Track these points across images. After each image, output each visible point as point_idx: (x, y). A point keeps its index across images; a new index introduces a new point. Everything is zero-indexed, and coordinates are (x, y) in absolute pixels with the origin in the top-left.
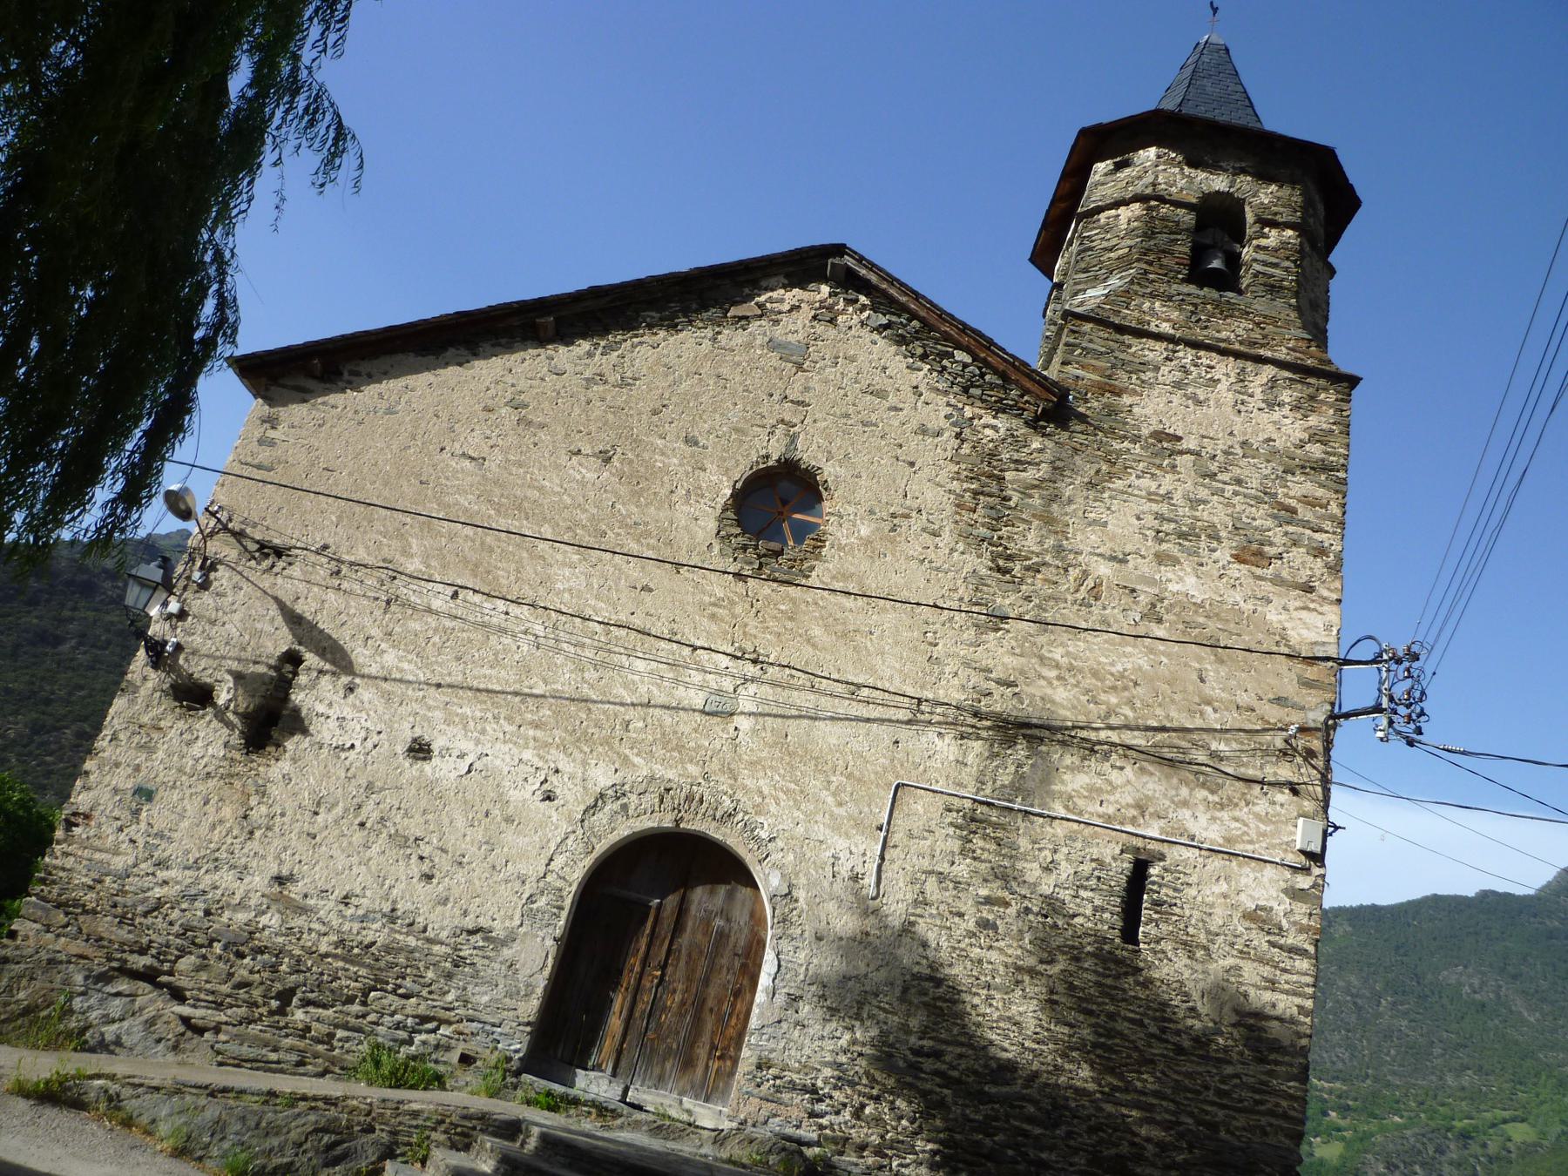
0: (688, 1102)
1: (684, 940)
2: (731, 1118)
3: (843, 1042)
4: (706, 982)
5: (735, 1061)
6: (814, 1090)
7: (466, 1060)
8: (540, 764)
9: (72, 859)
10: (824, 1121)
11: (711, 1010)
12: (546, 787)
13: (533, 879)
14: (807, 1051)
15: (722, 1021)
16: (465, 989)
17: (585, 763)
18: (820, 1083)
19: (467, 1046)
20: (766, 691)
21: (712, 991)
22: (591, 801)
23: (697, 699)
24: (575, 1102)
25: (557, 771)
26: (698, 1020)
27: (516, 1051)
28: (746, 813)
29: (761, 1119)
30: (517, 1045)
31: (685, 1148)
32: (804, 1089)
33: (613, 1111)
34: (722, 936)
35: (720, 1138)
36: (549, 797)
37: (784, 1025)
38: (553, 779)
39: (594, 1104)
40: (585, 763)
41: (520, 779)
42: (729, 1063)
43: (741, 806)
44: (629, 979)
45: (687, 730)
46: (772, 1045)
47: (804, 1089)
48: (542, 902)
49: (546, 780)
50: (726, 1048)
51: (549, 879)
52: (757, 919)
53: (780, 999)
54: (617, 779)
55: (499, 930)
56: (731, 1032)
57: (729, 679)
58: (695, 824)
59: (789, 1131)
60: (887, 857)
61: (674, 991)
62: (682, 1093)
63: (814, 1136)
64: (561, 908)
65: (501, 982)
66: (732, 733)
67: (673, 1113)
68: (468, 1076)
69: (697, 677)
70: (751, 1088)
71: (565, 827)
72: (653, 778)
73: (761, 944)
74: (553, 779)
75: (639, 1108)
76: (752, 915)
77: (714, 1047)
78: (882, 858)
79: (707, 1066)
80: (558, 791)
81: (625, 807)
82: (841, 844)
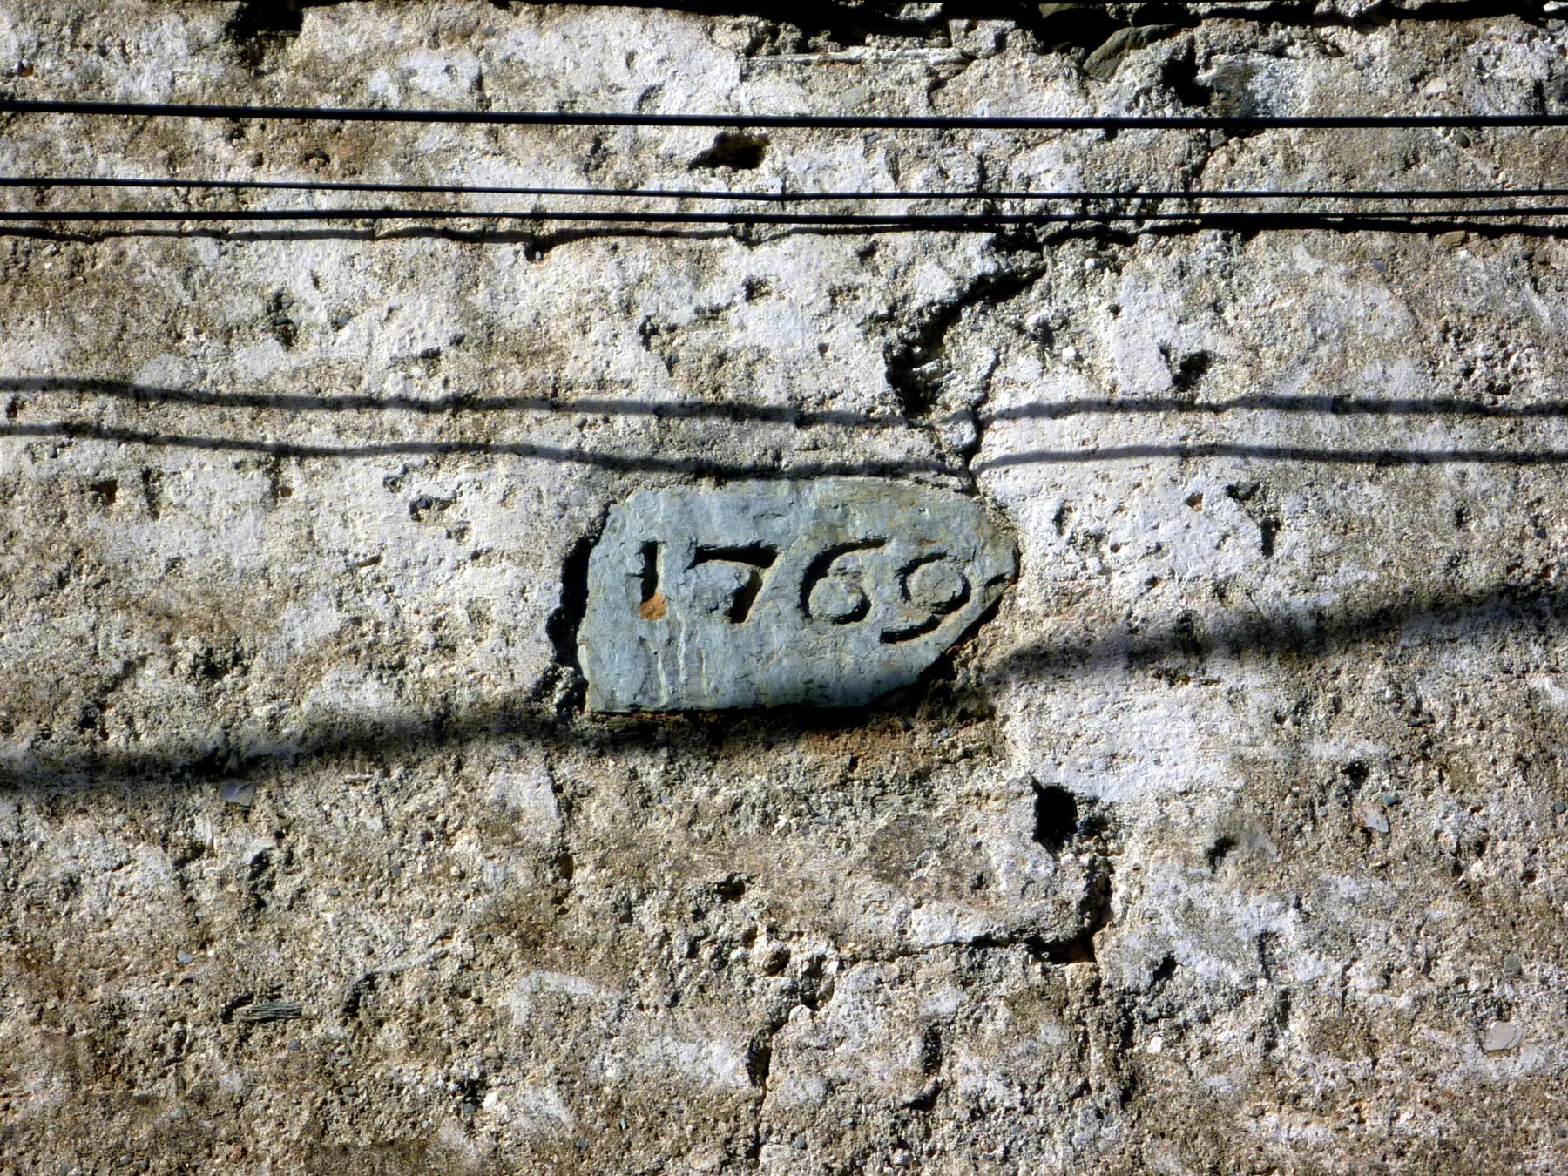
9: (824, 328)
20: (1312, 305)
23: (466, 572)
45: (408, 943)
57: (794, 262)
66: (1025, 878)
69: (376, 315)
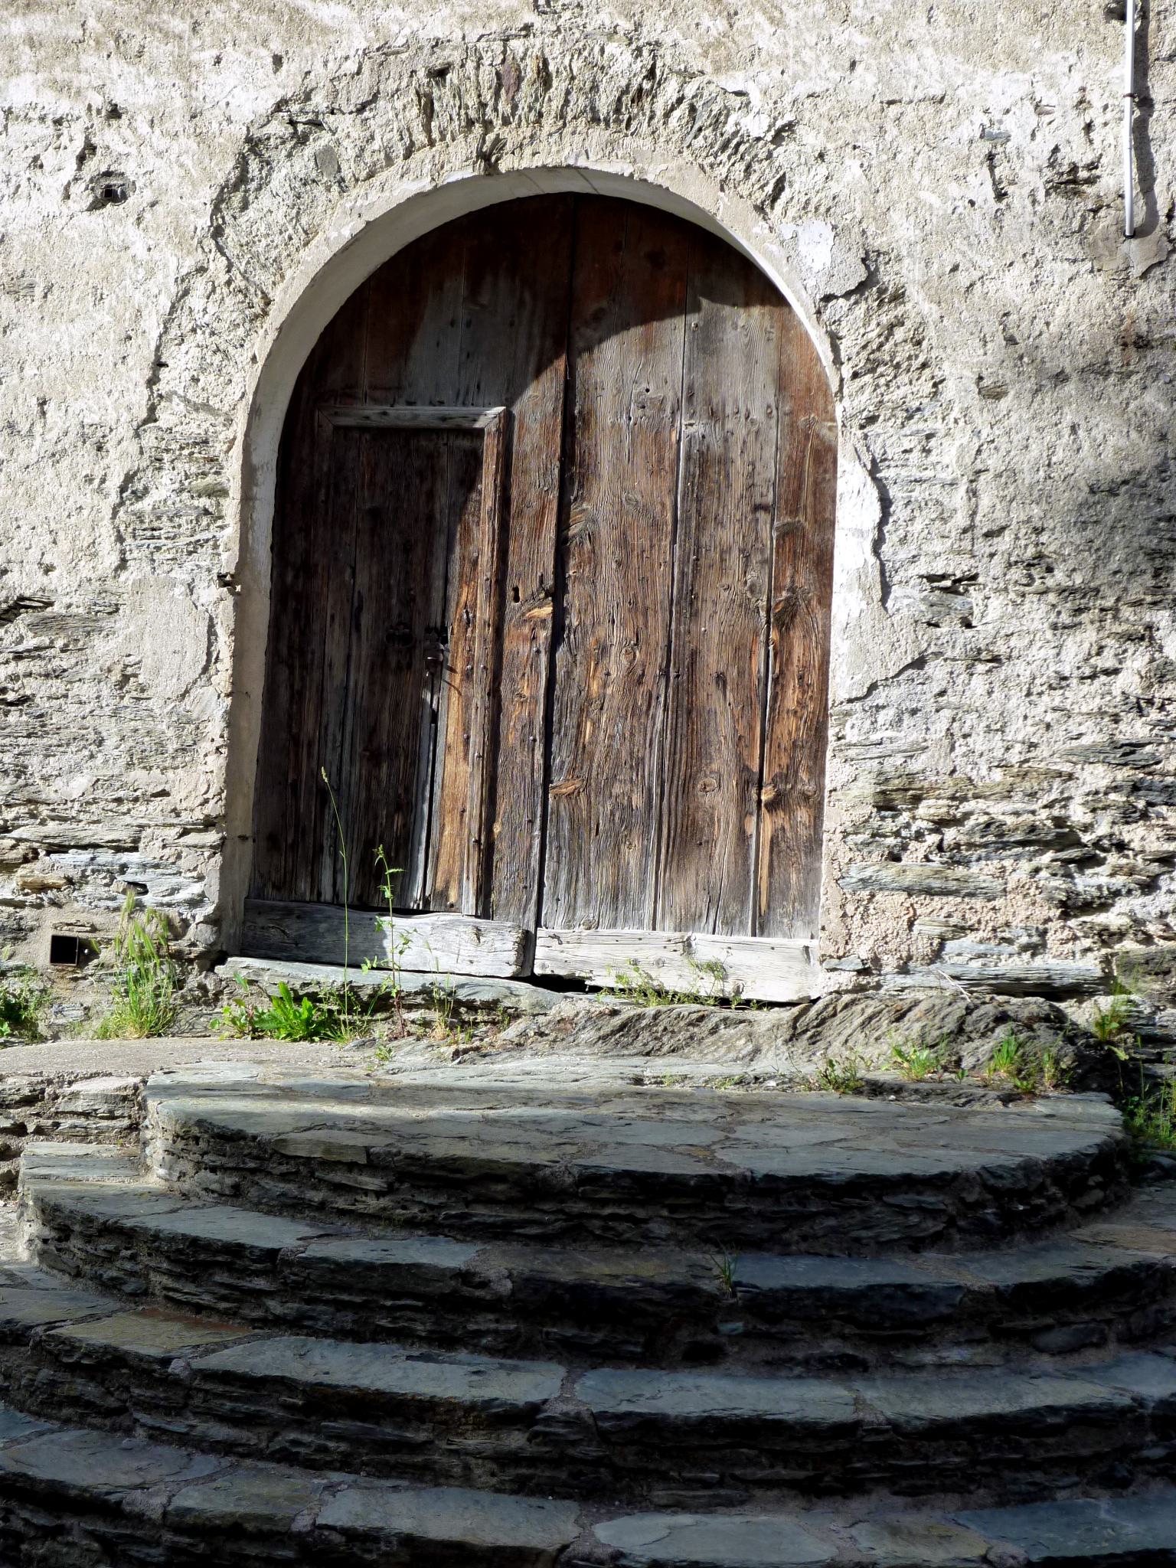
0: (708, 944)
1: (599, 506)
2: (833, 962)
3: (1129, 681)
4: (687, 602)
5: (815, 804)
6: (1063, 837)
7: (69, 951)
8: (63, 107)
10: (1113, 919)
11: (721, 679)
12: (95, 165)
13: (125, 431)
14: (1020, 730)
15: (764, 705)
16: (21, 771)
17: (185, 67)
18: (1078, 814)
19: (66, 915)
21: (713, 629)
22: (225, 169)
24: (382, 1003)
25: (115, 113)
26: (687, 713)
27: (195, 903)
28: (687, 75)
29: (922, 947)
30: (192, 882)
31: (704, 1067)
32: (1033, 840)
33: (490, 1006)
34: (706, 466)
35: (807, 1022)
36: (110, 195)
37: (936, 670)
38: (108, 137)
39: (427, 997)
40: (185, 67)
41: (20, 165)
42: (802, 815)
43: (666, 59)
44: (467, 648)
46: (910, 733)
47: (1033, 840)
48: (162, 489)
49: (90, 148)
50: (788, 775)
51: (165, 419)
52: (799, 393)
53: (909, 598)
54: (286, 82)
55: (68, 592)
56: (789, 728)
58: (556, 150)
59: (1013, 965)
60: (1158, 92)
61: (604, 650)
62: (687, 921)
63: (1090, 966)
64: (218, 492)
65: (110, 729)
67: (671, 980)
68: (86, 993)
70: (873, 866)
71: (173, 262)
72: (386, 51)
73: (825, 457)
74: (108, 137)
75: (572, 984)
76: (782, 381)
77: (750, 781)
78: (1143, 100)
79: (742, 837)
80: (129, 168)
81: (327, 159)
82: (998, 91)
